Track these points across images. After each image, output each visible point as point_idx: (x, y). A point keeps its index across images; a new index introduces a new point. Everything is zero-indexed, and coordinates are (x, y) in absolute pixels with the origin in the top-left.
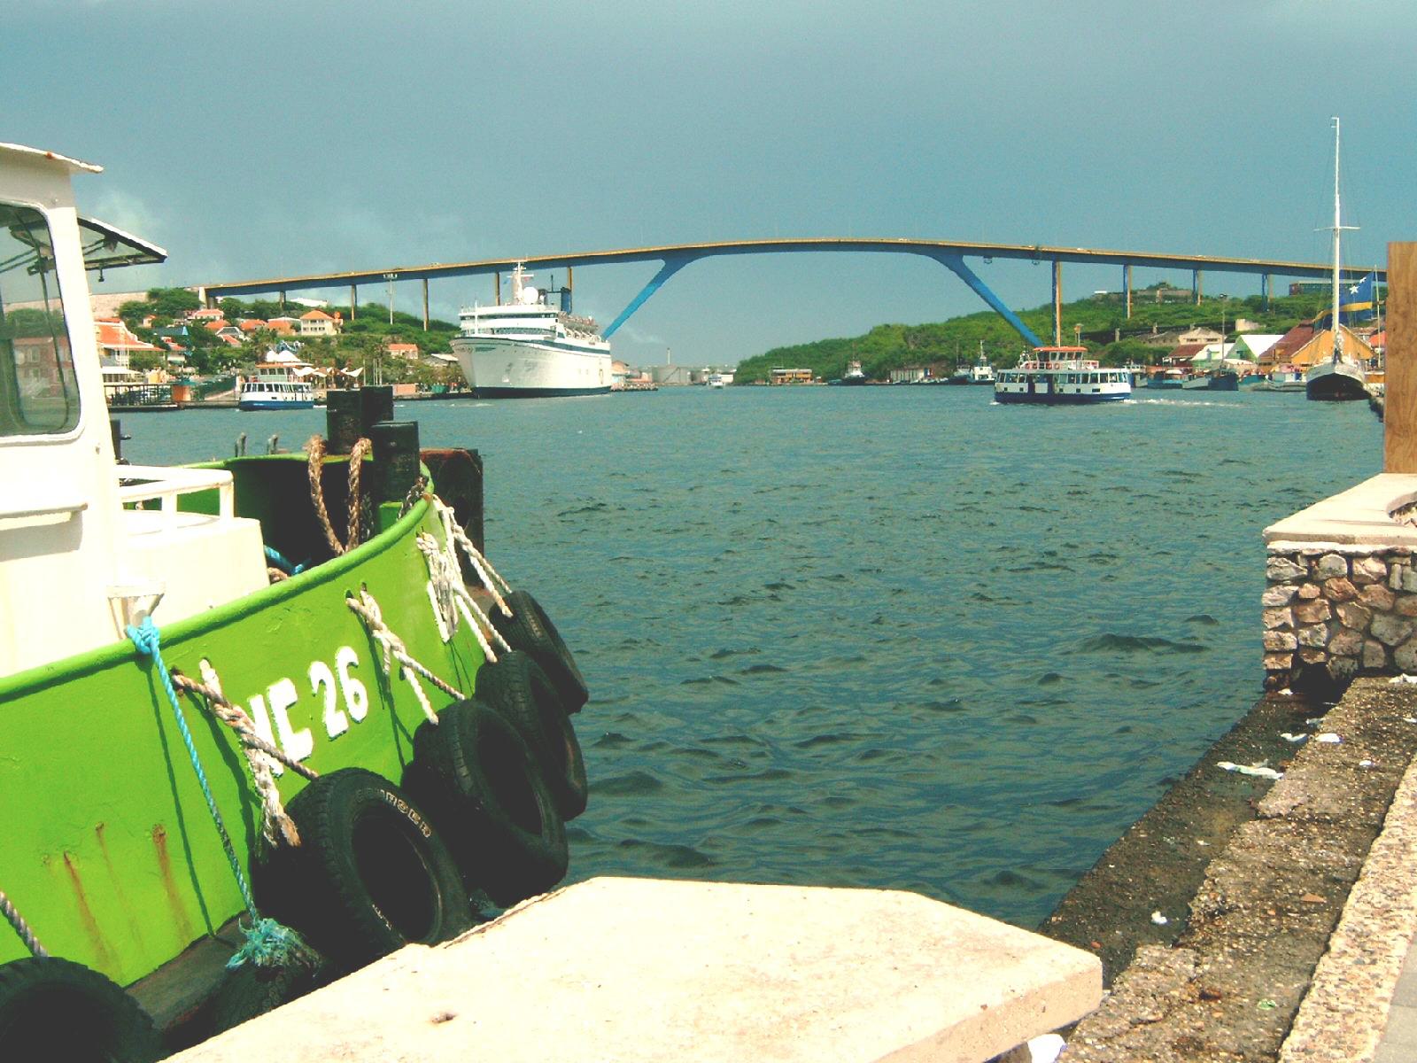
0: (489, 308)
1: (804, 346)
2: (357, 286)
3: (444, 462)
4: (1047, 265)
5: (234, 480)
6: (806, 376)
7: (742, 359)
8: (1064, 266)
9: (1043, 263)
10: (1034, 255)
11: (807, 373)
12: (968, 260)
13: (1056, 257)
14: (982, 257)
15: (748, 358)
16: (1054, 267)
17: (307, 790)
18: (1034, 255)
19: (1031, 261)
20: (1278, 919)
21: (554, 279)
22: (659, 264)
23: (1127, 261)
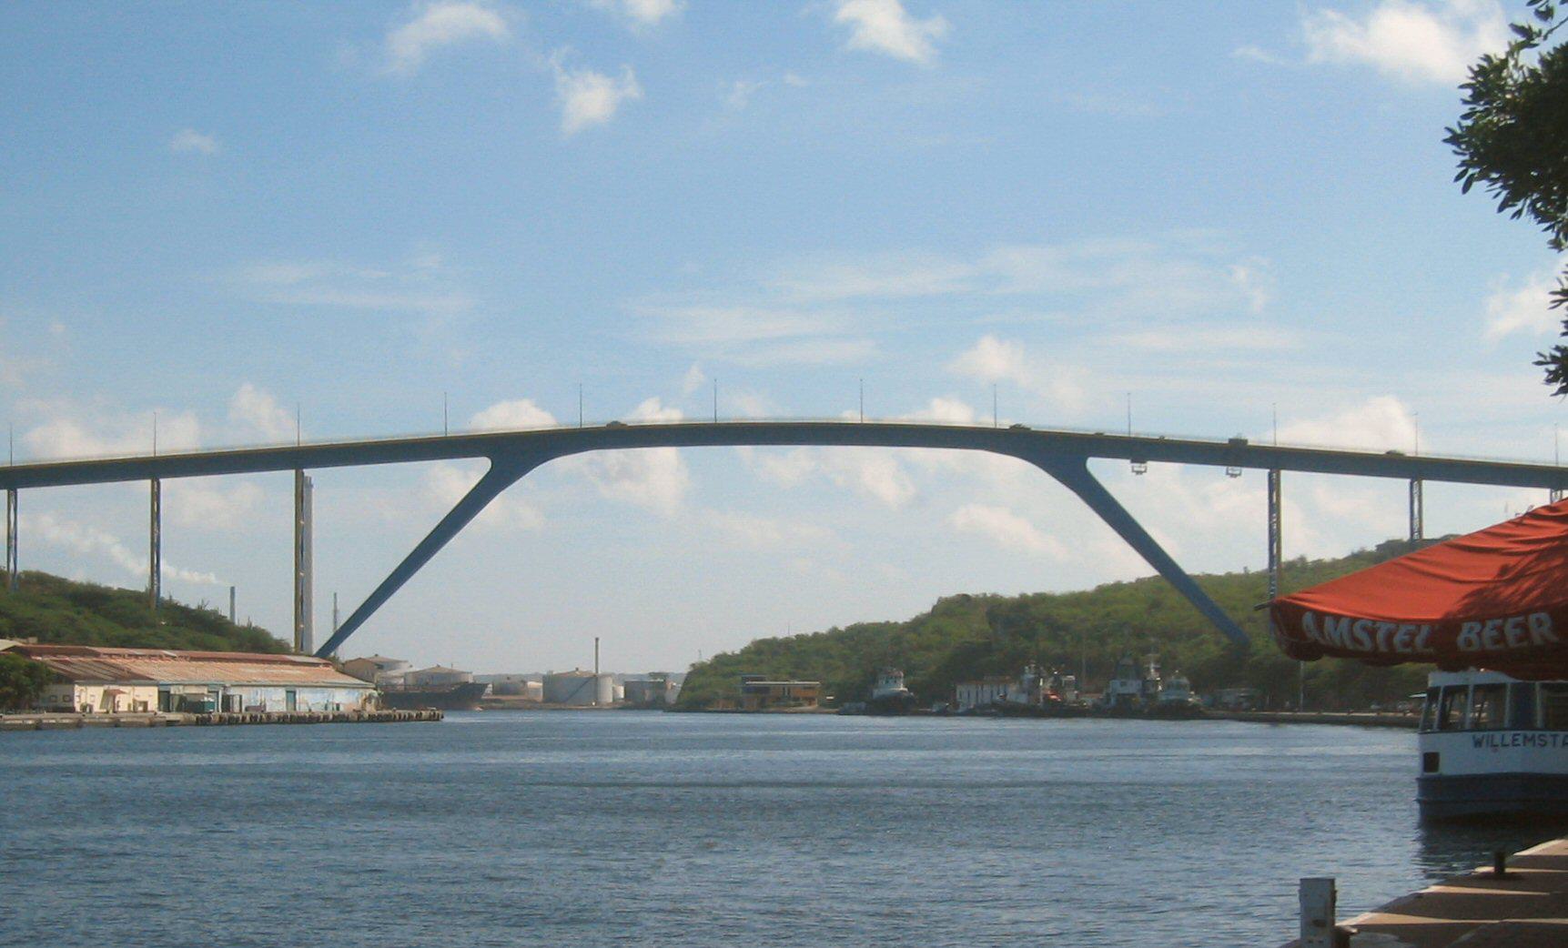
0: (1404, 922)
1: (816, 634)
2: (20, 491)
3: (1425, 630)
4: (1257, 478)
5: (1130, 438)
6: (810, 694)
7: (695, 660)
8: (1288, 478)
9: (1248, 472)
10: (1235, 454)
11: (811, 688)
12: (1098, 467)
13: (1277, 460)
14: (1128, 461)
15: (707, 657)
16: (1274, 487)
17: (135, 597)
18: (1235, 454)
19: (1224, 468)
20: (1461, 712)
21: (600, 642)
22: (480, 467)
23: (1416, 469)
